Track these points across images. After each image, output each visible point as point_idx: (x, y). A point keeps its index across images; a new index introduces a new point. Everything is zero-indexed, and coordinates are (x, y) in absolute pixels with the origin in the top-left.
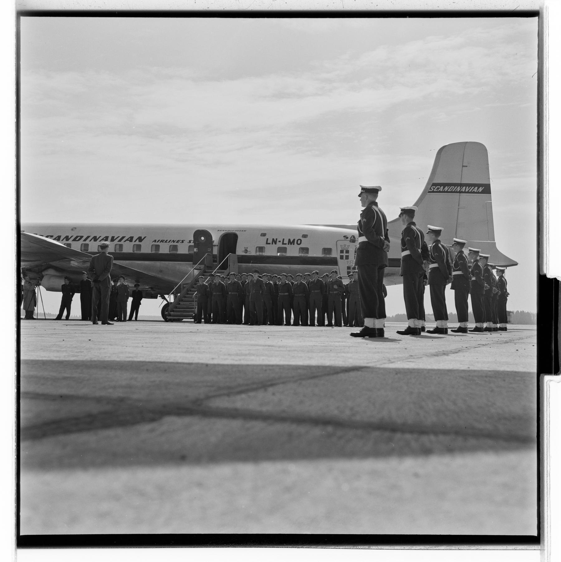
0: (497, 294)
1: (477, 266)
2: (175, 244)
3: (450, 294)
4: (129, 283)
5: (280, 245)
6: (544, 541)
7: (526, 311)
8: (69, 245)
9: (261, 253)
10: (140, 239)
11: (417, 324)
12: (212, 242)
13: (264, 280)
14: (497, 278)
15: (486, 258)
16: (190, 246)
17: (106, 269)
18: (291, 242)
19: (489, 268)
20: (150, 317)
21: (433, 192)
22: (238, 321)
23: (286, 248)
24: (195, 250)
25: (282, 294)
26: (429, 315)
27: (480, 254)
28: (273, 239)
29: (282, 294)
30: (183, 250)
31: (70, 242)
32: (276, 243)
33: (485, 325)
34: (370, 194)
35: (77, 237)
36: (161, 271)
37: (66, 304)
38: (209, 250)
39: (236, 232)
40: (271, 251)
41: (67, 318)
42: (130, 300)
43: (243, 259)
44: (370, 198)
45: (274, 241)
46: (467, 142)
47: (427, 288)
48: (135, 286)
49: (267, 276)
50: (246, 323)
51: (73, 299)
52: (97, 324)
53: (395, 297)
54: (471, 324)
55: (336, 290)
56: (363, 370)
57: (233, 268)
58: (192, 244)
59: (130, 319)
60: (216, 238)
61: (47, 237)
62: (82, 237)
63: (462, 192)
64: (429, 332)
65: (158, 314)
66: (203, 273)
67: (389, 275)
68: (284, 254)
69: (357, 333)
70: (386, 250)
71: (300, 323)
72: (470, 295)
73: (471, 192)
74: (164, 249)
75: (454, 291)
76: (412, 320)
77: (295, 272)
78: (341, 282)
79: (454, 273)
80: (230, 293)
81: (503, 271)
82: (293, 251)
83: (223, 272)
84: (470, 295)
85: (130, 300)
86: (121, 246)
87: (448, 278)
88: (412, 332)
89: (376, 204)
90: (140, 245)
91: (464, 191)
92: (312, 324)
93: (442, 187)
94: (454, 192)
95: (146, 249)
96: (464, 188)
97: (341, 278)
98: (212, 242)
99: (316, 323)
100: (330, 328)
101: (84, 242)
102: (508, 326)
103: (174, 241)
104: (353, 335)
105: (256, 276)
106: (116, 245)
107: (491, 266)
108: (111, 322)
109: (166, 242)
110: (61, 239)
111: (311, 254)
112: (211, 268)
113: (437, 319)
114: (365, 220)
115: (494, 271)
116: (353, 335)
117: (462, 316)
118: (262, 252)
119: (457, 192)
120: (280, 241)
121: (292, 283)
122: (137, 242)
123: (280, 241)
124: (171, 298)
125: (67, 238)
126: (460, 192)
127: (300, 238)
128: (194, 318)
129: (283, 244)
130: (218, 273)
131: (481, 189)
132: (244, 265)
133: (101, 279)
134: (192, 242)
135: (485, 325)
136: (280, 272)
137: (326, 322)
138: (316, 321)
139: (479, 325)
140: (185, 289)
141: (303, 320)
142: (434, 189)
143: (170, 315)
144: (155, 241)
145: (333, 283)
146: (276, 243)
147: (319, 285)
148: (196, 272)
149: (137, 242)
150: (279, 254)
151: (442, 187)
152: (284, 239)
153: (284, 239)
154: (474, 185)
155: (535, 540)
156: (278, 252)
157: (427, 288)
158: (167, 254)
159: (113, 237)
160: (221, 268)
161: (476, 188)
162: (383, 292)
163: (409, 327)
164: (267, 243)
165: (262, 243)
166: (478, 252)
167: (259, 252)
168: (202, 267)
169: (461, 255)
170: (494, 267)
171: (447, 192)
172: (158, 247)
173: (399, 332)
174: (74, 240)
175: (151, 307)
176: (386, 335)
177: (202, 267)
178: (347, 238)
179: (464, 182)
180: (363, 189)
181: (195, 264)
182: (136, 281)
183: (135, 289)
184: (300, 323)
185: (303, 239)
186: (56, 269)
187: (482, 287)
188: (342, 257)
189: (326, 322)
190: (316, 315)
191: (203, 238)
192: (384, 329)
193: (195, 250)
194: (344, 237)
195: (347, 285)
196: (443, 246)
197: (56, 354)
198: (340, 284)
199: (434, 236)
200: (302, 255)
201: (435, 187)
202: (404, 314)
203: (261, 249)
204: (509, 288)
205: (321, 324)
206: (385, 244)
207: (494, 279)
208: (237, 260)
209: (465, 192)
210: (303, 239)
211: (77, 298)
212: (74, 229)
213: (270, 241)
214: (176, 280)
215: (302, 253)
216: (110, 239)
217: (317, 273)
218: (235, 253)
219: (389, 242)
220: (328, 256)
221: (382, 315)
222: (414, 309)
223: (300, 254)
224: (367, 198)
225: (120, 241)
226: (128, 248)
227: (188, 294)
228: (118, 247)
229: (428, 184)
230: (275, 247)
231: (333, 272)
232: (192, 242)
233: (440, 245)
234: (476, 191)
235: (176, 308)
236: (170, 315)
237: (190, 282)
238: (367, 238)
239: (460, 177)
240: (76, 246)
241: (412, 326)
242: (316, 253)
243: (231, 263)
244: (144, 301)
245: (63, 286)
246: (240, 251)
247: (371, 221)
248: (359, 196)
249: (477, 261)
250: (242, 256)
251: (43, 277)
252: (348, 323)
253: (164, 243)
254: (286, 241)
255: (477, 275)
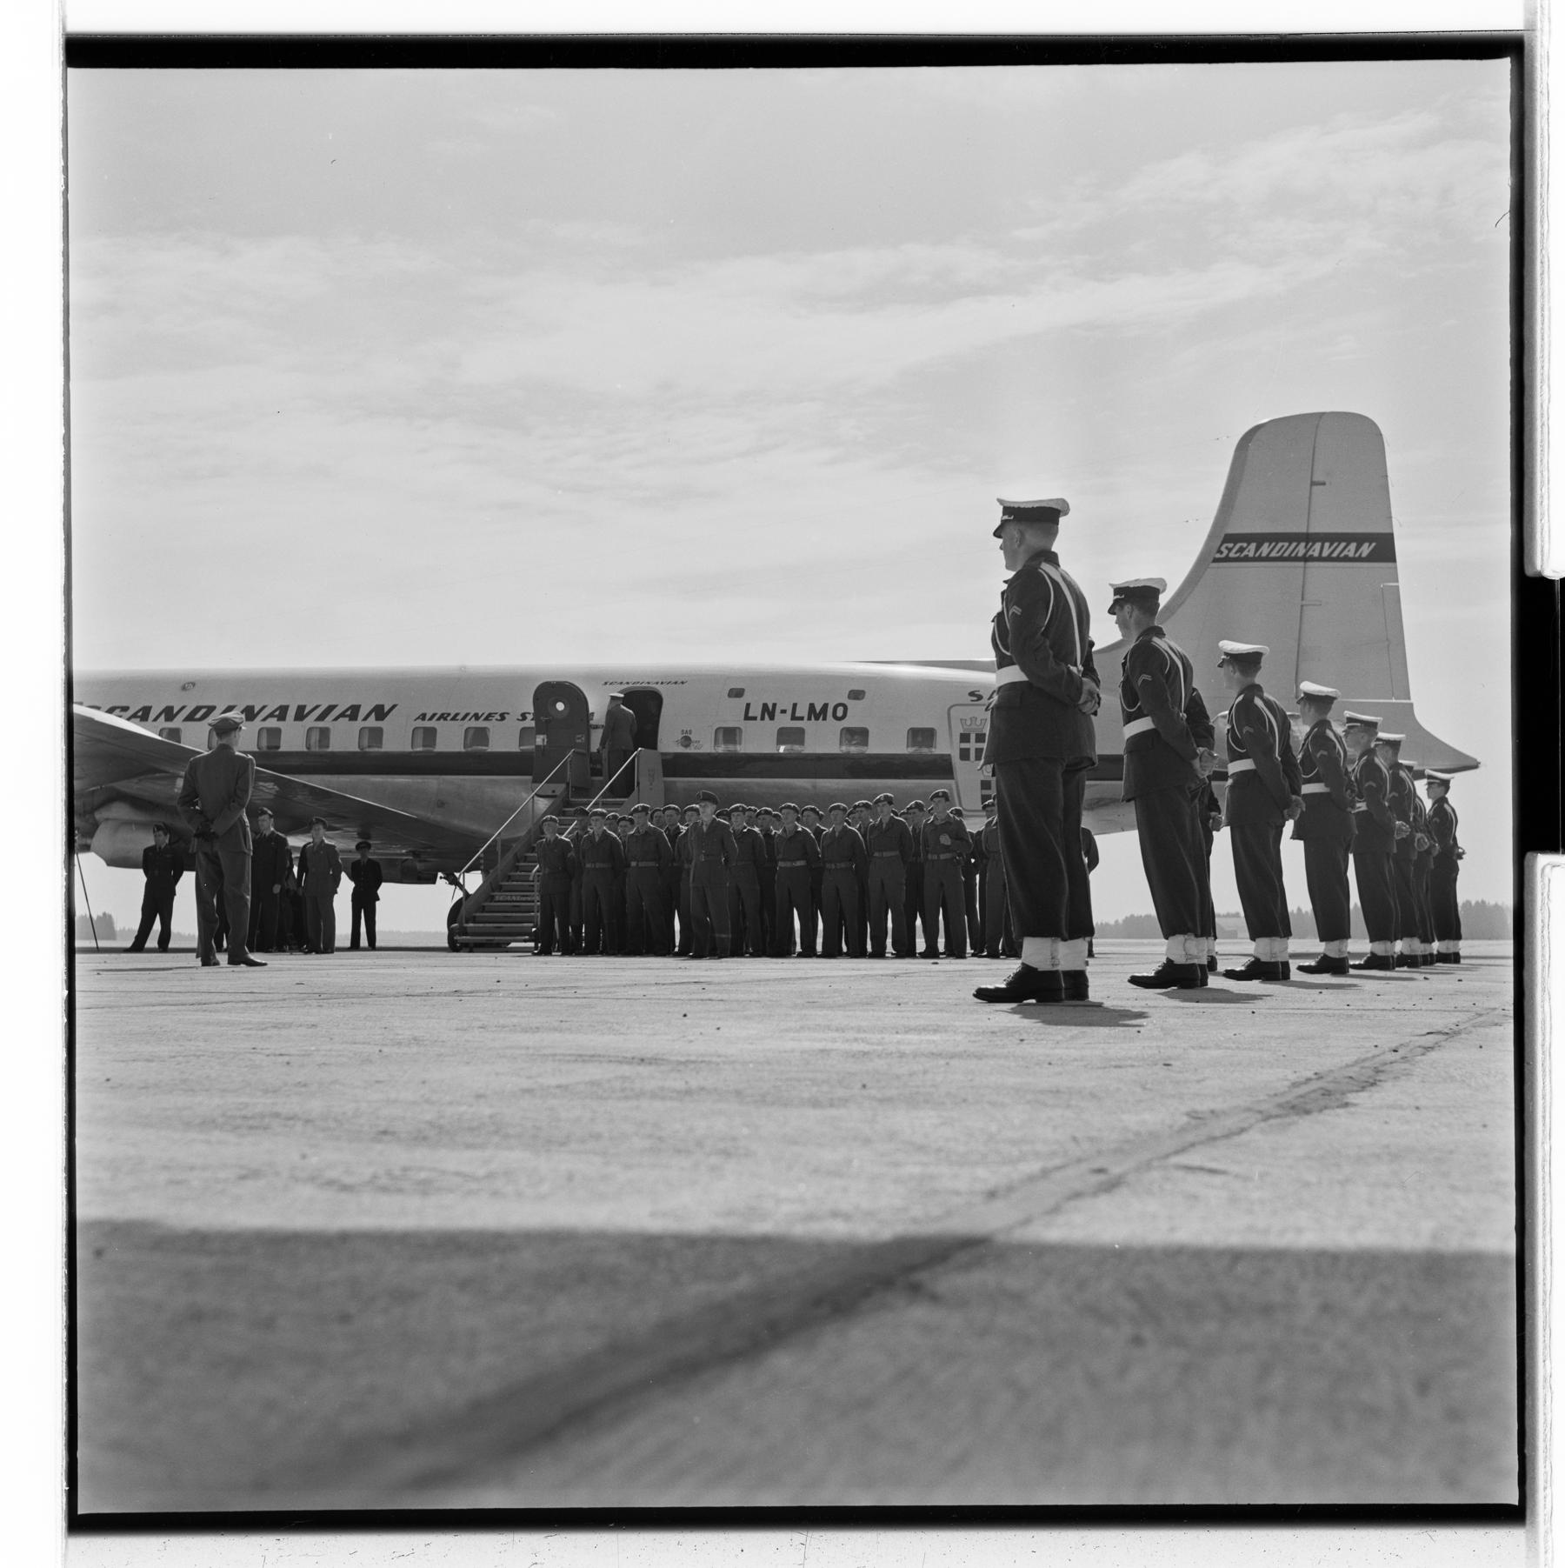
0: (1428, 852)
1: (1370, 769)
2: (481, 724)
3: (1292, 855)
4: (343, 842)
5: (784, 721)
6: (1534, 1514)
7: (1491, 901)
8: (175, 734)
9: (731, 748)
10: (380, 712)
11: (1194, 951)
12: (588, 716)
13: (739, 823)
14: (1428, 804)
15: (1395, 745)
16: (523, 730)
17: (234, 796)
18: (816, 713)
19: (1402, 774)
20: (417, 934)
21: (1227, 559)
22: (659, 946)
23: (801, 731)
24: (540, 740)
25: (788, 864)
26: (1228, 916)
27: (1381, 735)
28: (765, 706)
29: (788, 864)
30: (504, 740)
31: (177, 723)
32: (772, 717)
33: (1399, 947)
34: (1031, 525)
35: (198, 709)
36: (441, 804)
37: (158, 903)
38: (580, 739)
39: (659, 688)
40: (759, 740)
41: (164, 945)
42: (346, 886)
43: (676, 765)
44: (1033, 539)
45: (769, 712)
46: (1322, 414)
47: (1222, 840)
48: (358, 847)
49: (744, 810)
50: (683, 953)
51: (178, 888)
52: (217, 964)
53: (1119, 878)
54: (1359, 945)
55: (947, 849)
56: (948, 1281)
57: (650, 790)
58: (530, 723)
59: (355, 945)
60: (598, 705)
61: (111, 711)
62: (211, 709)
63: (1312, 559)
64: (1231, 974)
65: (438, 929)
66: (562, 807)
67: (1100, 803)
68: (797, 748)
69: (997, 989)
70: (1087, 708)
71: (845, 949)
72: (1351, 857)
73: (1338, 559)
74: (451, 740)
75: (1301, 843)
76: (1180, 938)
77: (825, 798)
78: (961, 826)
79: (1307, 789)
80: (633, 864)
81: (1445, 784)
82: (823, 740)
83: (620, 804)
84: (1351, 857)
85: (346, 886)
86: (325, 733)
87: (1287, 804)
88: (1179, 978)
89: (1053, 559)
90: (380, 730)
91: (1316, 554)
92: (879, 953)
93: (1253, 546)
94: (1289, 559)
95: (397, 740)
96: (1318, 546)
97: (958, 813)
98: (589, 716)
99: (889, 948)
100: (926, 964)
101: (321, 724)
102: (1464, 947)
103: (477, 717)
104: (986, 995)
105: (707, 813)
106: (310, 729)
107: (1410, 768)
108: (254, 957)
109: (454, 719)
110: (152, 715)
111: (874, 748)
112: (585, 791)
113: (1254, 936)
114: (1016, 610)
115: (1421, 787)
116: (986, 995)
117: (1332, 924)
118: (734, 742)
119: (1296, 559)
120: (783, 712)
121: (818, 832)
122: (372, 722)
123: (783, 712)
124: (473, 881)
125: (169, 713)
126: (1306, 559)
127: (841, 699)
128: (534, 938)
129: (794, 718)
130: (604, 805)
131: (1366, 549)
132: (681, 782)
133: (218, 827)
134: (530, 717)
135: (1399, 947)
136: (775, 799)
137: (921, 945)
138: (889, 941)
139: (1380, 948)
140: (510, 856)
141: (851, 938)
142: (1230, 550)
143: (470, 931)
144: (423, 717)
145: (937, 829)
146: (772, 717)
147: (894, 834)
148: (543, 804)
149: (372, 722)
150: (782, 749)
151: (1253, 546)
152: (795, 705)
153: (795, 705)
154: (1347, 538)
155: (1514, 1515)
156: (780, 742)
157: (1222, 840)
158: (459, 753)
159: (301, 709)
160: (612, 791)
161: (1353, 546)
162: (1082, 855)
163: (1169, 961)
164: (747, 718)
165: (733, 719)
166: (1373, 725)
167: (726, 742)
168: (560, 788)
169: (1319, 736)
170: (1420, 775)
171: (1268, 559)
172: (430, 734)
173: (1136, 981)
174: (190, 718)
175: (416, 909)
176: (1094, 995)
177: (560, 788)
178: (980, 698)
179: (1317, 528)
180: (1008, 510)
181: (537, 781)
182: (360, 835)
183: (358, 856)
184: (845, 949)
185: (850, 704)
186: (136, 802)
187: (1389, 831)
188: (964, 755)
189: (921, 945)
190: (890, 925)
191: (560, 706)
192: (1089, 970)
193: (540, 740)
194: (972, 694)
195: (979, 833)
196: (1268, 703)
197: (501, 973)
198: (958, 831)
199: (1237, 674)
200: (853, 750)
201: (1230, 546)
202: (1148, 917)
203: (730, 734)
204: (1463, 836)
205: (905, 950)
206: (1086, 688)
207: (1418, 809)
208: (660, 768)
209: (1320, 559)
210: (850, 704)
211: (187, 885)
212: (188, 686)
213: (756, 711)
214: (486, 830)
215: (850, 743)
216: (291, 713)
217: (889, 801)
218: (654, 746)
219: (1097, 682)
220: (925, 751)
221: (1080, 925)
222: (1182, 907)
223: (844, 749)
224: (1022, 540)
225: (321, 718)
226: (345, 739)
227: (517, 869)
228: (315, 737)
229: (1211, 537)
230: (770, 728)
231: (937, 795)
232: (530, 717)
233: (1258, 702)
234: (1351, 554)
235: (483, 909)
236: (470, 931)
237: (523, 834)
238: (1023, 669)
239: (1305, 509)
240: (197, 739)
241: (1179, 959)
242: (888, 742)
243: (642, 779)
244: (386, 890)
245: (147, 851)
246: (669, 743)
247: (1036, 614)
248: (997, 534)
249: (1370, 752)
250: (677, 755)
251: (96, 826)
252: (986, 948)
253: (449, 723)
254: (802, 711)
255: (1374, 796)
